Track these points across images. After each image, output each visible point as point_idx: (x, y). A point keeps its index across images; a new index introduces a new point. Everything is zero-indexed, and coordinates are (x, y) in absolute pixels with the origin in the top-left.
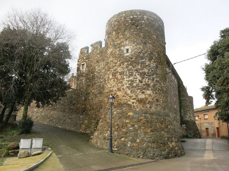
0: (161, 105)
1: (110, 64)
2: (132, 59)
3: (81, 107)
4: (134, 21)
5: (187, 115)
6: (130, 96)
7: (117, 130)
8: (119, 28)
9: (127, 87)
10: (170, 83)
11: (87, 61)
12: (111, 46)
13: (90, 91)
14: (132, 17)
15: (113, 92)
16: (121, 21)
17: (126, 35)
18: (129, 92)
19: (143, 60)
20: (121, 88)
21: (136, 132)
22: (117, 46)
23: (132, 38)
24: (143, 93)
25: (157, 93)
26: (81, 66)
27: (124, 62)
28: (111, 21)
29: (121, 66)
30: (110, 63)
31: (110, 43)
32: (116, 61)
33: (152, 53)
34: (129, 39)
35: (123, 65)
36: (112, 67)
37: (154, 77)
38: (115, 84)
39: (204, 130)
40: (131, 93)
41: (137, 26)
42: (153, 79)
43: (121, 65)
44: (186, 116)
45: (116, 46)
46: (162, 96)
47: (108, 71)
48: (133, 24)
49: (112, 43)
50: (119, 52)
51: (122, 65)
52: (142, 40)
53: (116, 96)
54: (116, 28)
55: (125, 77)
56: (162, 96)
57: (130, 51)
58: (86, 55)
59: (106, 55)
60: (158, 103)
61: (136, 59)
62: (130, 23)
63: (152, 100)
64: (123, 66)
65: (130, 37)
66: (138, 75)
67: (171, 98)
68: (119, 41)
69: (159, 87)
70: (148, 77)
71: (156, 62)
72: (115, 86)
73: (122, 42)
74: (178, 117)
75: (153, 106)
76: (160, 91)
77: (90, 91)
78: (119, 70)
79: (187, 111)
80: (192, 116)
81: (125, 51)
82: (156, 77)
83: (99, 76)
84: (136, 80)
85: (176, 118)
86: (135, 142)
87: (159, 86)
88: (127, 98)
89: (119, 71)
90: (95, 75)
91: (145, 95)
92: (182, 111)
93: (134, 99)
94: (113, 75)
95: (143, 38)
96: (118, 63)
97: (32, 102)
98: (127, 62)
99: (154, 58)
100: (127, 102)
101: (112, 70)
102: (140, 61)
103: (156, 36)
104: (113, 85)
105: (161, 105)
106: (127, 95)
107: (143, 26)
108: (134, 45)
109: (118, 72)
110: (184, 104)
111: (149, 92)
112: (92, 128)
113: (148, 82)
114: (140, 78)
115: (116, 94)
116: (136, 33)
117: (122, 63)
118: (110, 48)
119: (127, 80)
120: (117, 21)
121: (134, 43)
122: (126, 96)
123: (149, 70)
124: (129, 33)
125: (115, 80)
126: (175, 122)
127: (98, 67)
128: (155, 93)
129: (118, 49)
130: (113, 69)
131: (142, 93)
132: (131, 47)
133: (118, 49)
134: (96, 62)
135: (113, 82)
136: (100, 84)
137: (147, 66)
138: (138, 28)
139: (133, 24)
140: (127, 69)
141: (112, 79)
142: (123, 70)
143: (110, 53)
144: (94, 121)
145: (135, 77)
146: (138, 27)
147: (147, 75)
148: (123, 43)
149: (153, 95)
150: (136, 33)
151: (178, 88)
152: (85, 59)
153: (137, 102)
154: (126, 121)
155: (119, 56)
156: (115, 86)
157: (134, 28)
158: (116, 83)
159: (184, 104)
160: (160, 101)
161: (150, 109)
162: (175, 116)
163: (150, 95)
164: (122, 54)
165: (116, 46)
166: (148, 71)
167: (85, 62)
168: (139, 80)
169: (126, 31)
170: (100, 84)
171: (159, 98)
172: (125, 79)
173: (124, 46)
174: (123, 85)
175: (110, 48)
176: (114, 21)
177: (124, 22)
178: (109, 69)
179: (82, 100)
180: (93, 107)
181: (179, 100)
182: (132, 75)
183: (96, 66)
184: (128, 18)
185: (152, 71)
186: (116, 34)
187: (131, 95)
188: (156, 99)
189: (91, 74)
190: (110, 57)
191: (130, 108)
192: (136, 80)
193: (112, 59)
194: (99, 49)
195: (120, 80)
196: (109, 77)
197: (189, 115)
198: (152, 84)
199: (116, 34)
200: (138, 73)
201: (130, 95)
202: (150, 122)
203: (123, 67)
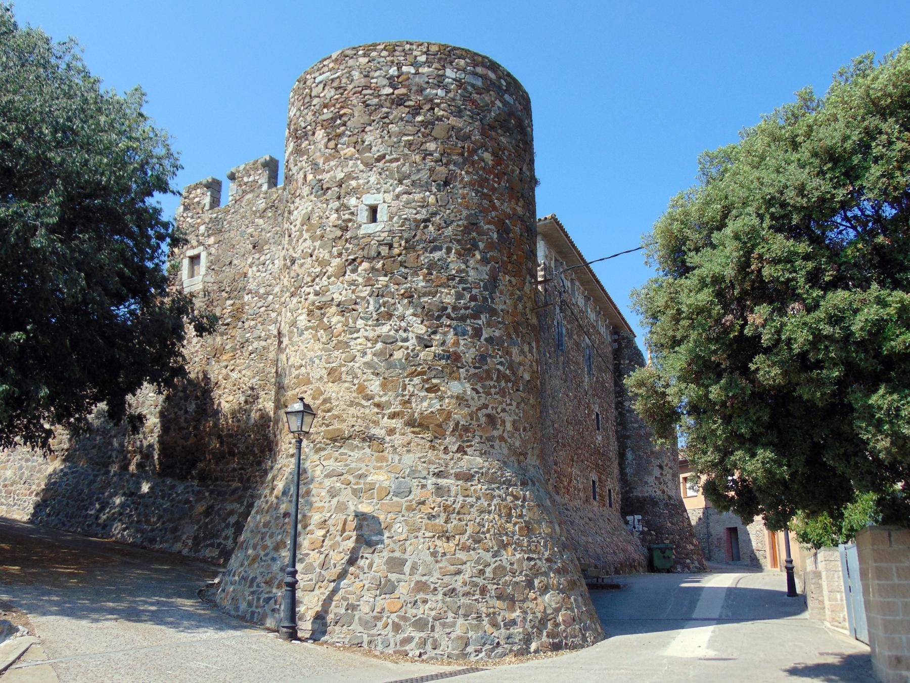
0: (506, 442)
1: (302, 265)
2: (391, 246)
3: (181, 442)
4: (402, 91)
5: (650, 474)
6: (378, 405)
7: (322, 546)
8: (341, 117)
9: (368, 365)
10: (575, 337)
11: (212, 240)
12: (306, 190)
13: (220, 377)
14: (393, 71)
15: (312, 383)
16: (350, 87)
17: (370, 147)
18: (374, 386)
19: (437, 255)
20: (343, 369)
21: (397, 554)
22: (330, 192)
23: (391, 161)
24: (433, 389)
25: (493, 391)
26: (186, 262)
27: (359, 260)
28: (308, 83)
29: (347, 277)
30: (303, 261)
31: (301, 175)
32: (327, 256)
33: (473, 224)
34: (381, 164)
35: (354, 271)
36: (309, 279)
37: (480, 322)
38: (319, 353)
39: (721, 539)
40: (381, 393)
41: (416, 110)
42: (477, 333)
43: (345, 273)
45: (328, 189)
46: (514, 404)
47: (293, 295)
48: (400, 102)
49: (310, 177)
50: (339, 218)
51: (348, 272)
52: (432, 170)
53: (322, 404)
54: (330, 115)
55: (360, 323)
56: (511, 404)
57: (382, 215)
58: (207, 216)
59: (286, 226)
60: (496, 433)
61: (405, 248)
62: (387, 95)
63: (469, 418)
64: (354, 276)
65: (384, 157)
66: (414, 315)
67: (580, 402)
68: (339, 169)
69: (499, 367)
70: (455, 323)
71: (488, 263)
72: (317, 361)
73: (349, 177)
74: (613, 484)
75: (471, 446)
76: (503, 384)
77: (220, 377)
78: (339, 292)
79: (648, 456)
80: (669, 477)
81: (363, 216)
82: (489, 325)
83: (263, 309)
84: (405, 335)
85: (602, 486)
86: (392, 596)
87: (501, 363)
88: (367, 411)
89: (335, 296)
90: (243, 305)
91: (441, 398)
92: (629, 455)
93: (393, 416)
94: (310, 313)
95: (436, 161)
96: (336, 262)
98: (370, 259)
99: (481, 245)
100: (367, 427)
101: (308, 290)
102: (424, 259)
103: (494, 154)
104: (310, 354)
105: (506, 442)
106: (368, 398)
107: (442, 113)
108: (399, 189)
109: (333, 299)
110: (636, 425)
111: (455, 387)
112: (226, 538)
113: (457, 343)
114: (421, 330)
115: (322, 393)
116: (411, 138)
117: (349, 264)
118: (303, 197)
119: (366, 334)
120: (335, 84)
121: (400, 182)
122: (364, 402)
123: (459, 296)
124: (381, 137)
125: (319, 335)
126: (595, 503)
127: (258, 271)
128: (481, 390)
129: (337, 204)
130: (311, 290)
131: (428, 390)
132: (389, 197)
133: (337, 204)
134: (251, 246)
135: (312, 341)
136: (263, 343)
137: (453, 278)
138: (419, 118)
139: (400, 102)
140: (369, 288)
141: (307, 329)
142: (353, 292)
143: (300, 220)
144: (235, 506)
145: (403, 324)
146: (418, 114)
147: (453, 315)
148: (357, 178)
149: (473, 399)
150: (411, 138)
151: (615, 359)
152: (203, 235)
153: (409, 430)
154: (360, 506)
155: (339, 233)
156: (317, 361)
157: (402, 119)
158: (323, 349)
159: (636, 425)
160: (503, 422)
161: (459, 455)
163: (461, 399)
164: (350, 224)
165: (328, 189)
166: (457, 299)
167: (202, 248)
168: (419, 338)
169: (368, 128)
170: (263, 343)
171: (499, 410)
172: (358, 331)
173: (356, 192)
174: (353, 359)
175: (303, 197)
176: (321, 86)
177: (360, 92)
178: (297, 288)
179: (186, 412)
180: (235, 445)
181: (616, 409)
182: (389, 316)
183: (251, 267)
184: (378, 73)
185: (473, 298)
186: (329, 140)
187: (384, 399)
188: (488, 416)
189: (229, 302)
190: (301, 235)
191: (376, 454)
192: (405, 335)
193: (309, 242)
194: (266, 193)
195: (340, 335)
196: (294, 323)
197: (657, 472)
198: (470, 355)
199: (329, 140)
200: (415, 307)
201: (377, 399)
202: (458, 513)
203: (353, 283)
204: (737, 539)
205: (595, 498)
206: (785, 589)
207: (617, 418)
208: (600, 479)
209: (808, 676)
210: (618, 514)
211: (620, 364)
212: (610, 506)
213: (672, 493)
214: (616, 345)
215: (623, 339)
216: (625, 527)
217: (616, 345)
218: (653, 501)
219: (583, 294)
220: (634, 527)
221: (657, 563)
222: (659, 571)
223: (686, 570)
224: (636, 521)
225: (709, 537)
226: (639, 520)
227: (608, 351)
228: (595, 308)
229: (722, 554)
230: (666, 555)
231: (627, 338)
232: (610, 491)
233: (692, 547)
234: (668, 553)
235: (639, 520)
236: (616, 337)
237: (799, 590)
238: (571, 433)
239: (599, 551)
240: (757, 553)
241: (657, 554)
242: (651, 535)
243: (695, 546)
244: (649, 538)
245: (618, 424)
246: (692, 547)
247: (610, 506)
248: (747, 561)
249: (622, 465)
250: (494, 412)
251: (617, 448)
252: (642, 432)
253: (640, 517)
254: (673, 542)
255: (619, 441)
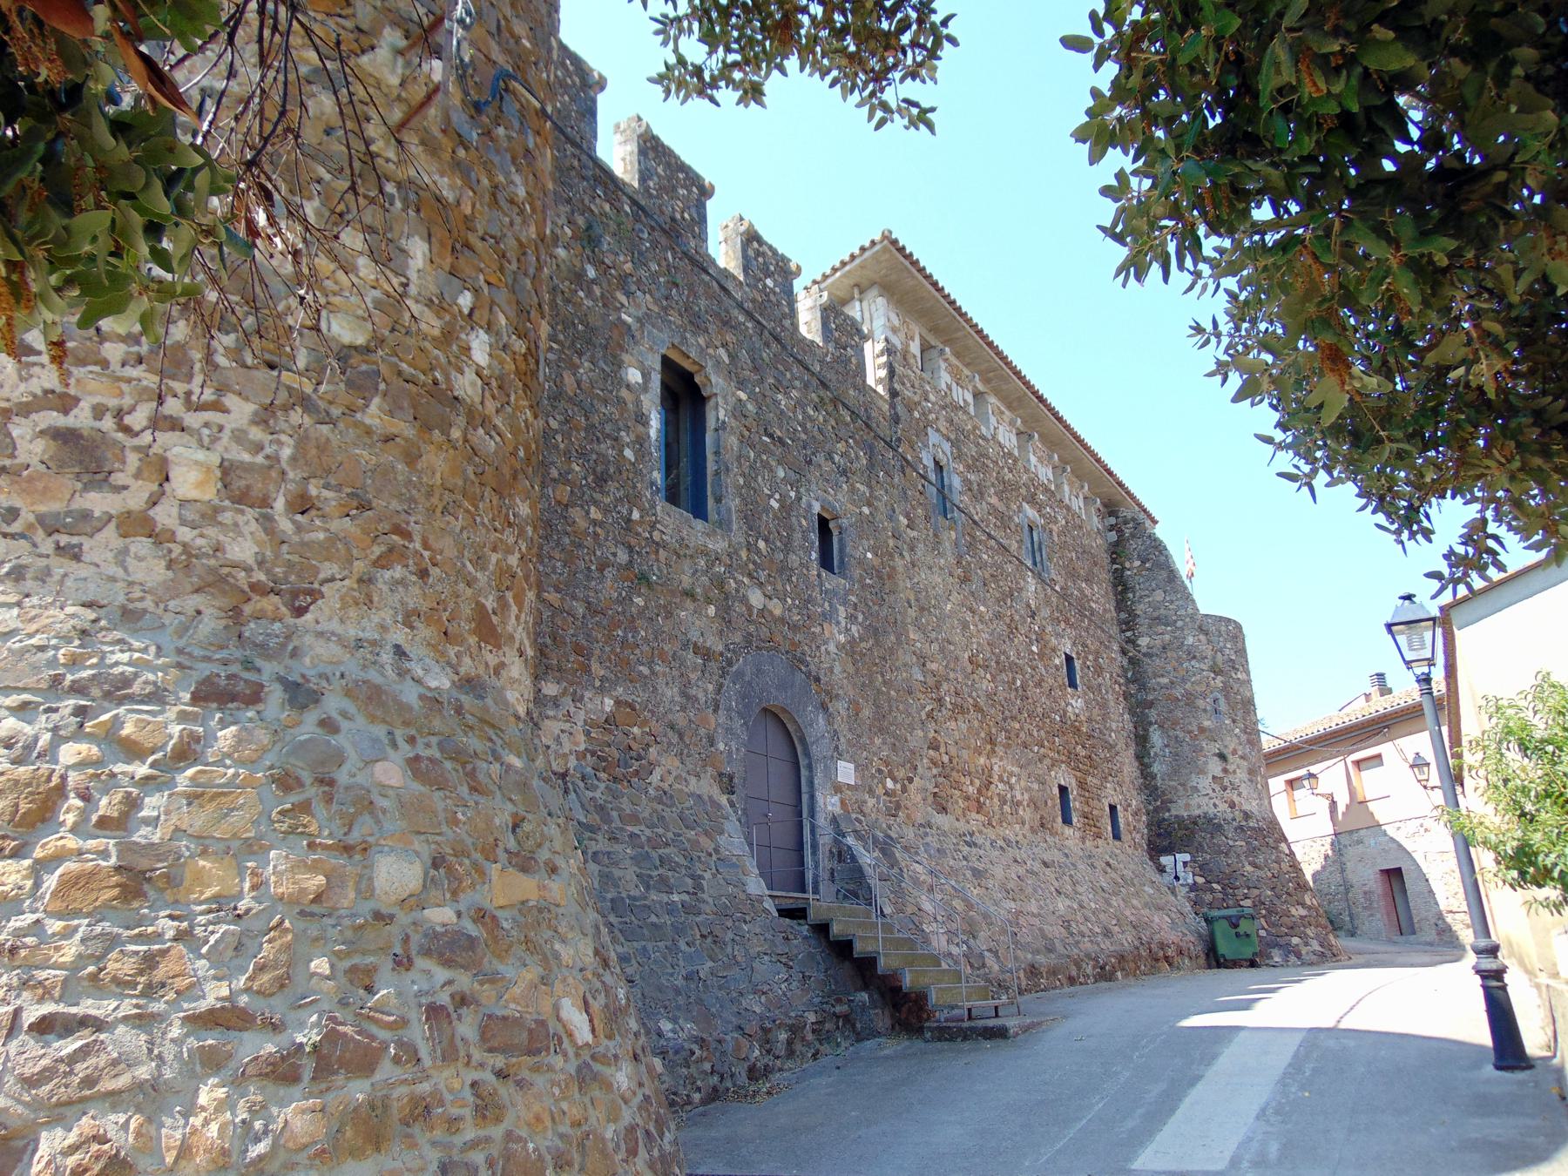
5: (1202, 772)
44: (1194, 780)
79: (1195, 738)
80: (1241, 775)
92: (1156, 738)
97: (1465, 61)
110: (1165, 681)
126: (1068, 831)
136: (532, 271)
151: (1113, 561)
159: (1165, 681)
162: (1070, 781)
171: (138, 419)
197: (1215, 767)
204: (1404, 891)
205: (1067, 821)
206: (1481, 1034)
207: (1125, 671)
208: (1082, 785)
209: (1540, 570)
210: (1141, 854)
211: (1124, 568)
212: (1117, 836)
213: (1252, 806)
214: (1113, 536)
215: (1126, 523)
216: (1156, 877)
217: (1113, 536)
218: (1213, 826)
219: (1012, 423)
220: (1177, 878)
221: (1224, 948)
222: (1234, 964)
223: (1293, 958)
224: (1180, 866)
225: (1347, 891)
226: (1185, 864)
227: (1098, 545)
228: (1051, 457)
229: (1377, 920)
230: (1241, 930)
231: (1133, 519)
232: (1113, 808)
233: (1303, 912)
234: (1244, 926)
235: (1185, 864)
236: (1113, 520)
237: (1533, 1041)
238: (986, 685)
239: (1055, 931)
240: (1449, 919)
241: (1221, 928)
242: (1212, 891)
243: (1309, 908)
244: (1208, 897)
245: (1128, 681)
246: (1303, 912)
247: (1117, 836)
248: (1431, 935)
249: (1143, 757)
250: (108, 423)
251: (1130, 726)
252: (1178, 692)
253: (1187, 857)
254: (1259, 903)
255: (1132, 713)
